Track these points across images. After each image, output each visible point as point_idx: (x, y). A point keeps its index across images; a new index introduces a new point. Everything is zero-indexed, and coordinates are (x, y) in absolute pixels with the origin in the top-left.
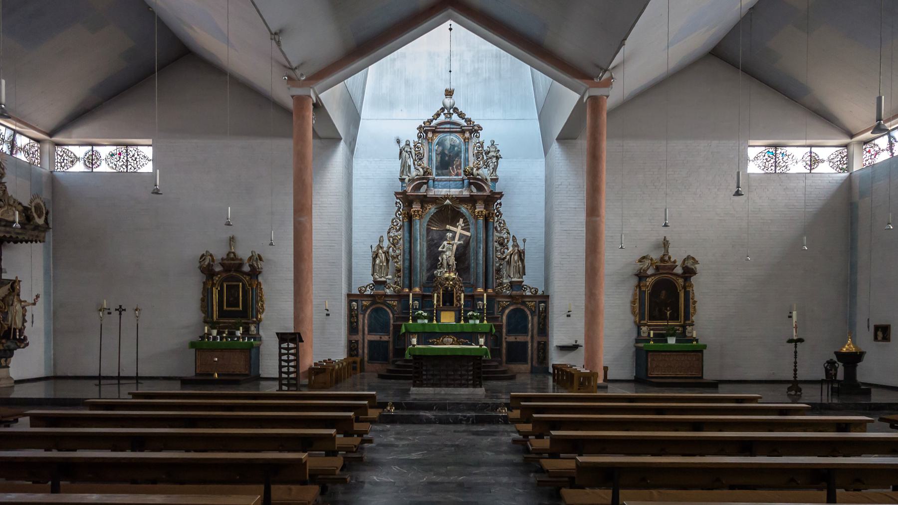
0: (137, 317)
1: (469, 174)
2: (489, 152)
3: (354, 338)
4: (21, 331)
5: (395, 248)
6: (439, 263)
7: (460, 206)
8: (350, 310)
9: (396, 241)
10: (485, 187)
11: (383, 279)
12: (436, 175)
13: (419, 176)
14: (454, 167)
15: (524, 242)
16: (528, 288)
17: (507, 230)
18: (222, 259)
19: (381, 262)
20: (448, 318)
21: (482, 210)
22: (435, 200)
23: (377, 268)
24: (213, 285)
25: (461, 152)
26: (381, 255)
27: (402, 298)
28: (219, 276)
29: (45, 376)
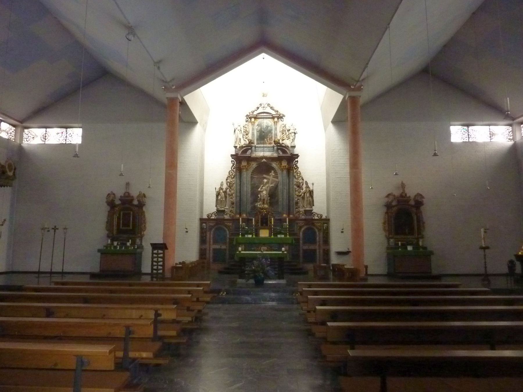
1: (277, 143)
2: (290, 130)
3: (204, 247)
6: (259, 199)
7: (272, 163)
9: (231, 185)
11: (223, 209)
12: (257, 144)
14: (268, 139)
15: (313, 185)
16: (316, 214)
17: (302, 177)
18: (121, 197)
19: (222, 198)
20: (264, 233)
22: (256, 159)
23: (219, 202)
25: (272, 130)
26: (222, 194)
27: (235, 221)
28: (118, 207)
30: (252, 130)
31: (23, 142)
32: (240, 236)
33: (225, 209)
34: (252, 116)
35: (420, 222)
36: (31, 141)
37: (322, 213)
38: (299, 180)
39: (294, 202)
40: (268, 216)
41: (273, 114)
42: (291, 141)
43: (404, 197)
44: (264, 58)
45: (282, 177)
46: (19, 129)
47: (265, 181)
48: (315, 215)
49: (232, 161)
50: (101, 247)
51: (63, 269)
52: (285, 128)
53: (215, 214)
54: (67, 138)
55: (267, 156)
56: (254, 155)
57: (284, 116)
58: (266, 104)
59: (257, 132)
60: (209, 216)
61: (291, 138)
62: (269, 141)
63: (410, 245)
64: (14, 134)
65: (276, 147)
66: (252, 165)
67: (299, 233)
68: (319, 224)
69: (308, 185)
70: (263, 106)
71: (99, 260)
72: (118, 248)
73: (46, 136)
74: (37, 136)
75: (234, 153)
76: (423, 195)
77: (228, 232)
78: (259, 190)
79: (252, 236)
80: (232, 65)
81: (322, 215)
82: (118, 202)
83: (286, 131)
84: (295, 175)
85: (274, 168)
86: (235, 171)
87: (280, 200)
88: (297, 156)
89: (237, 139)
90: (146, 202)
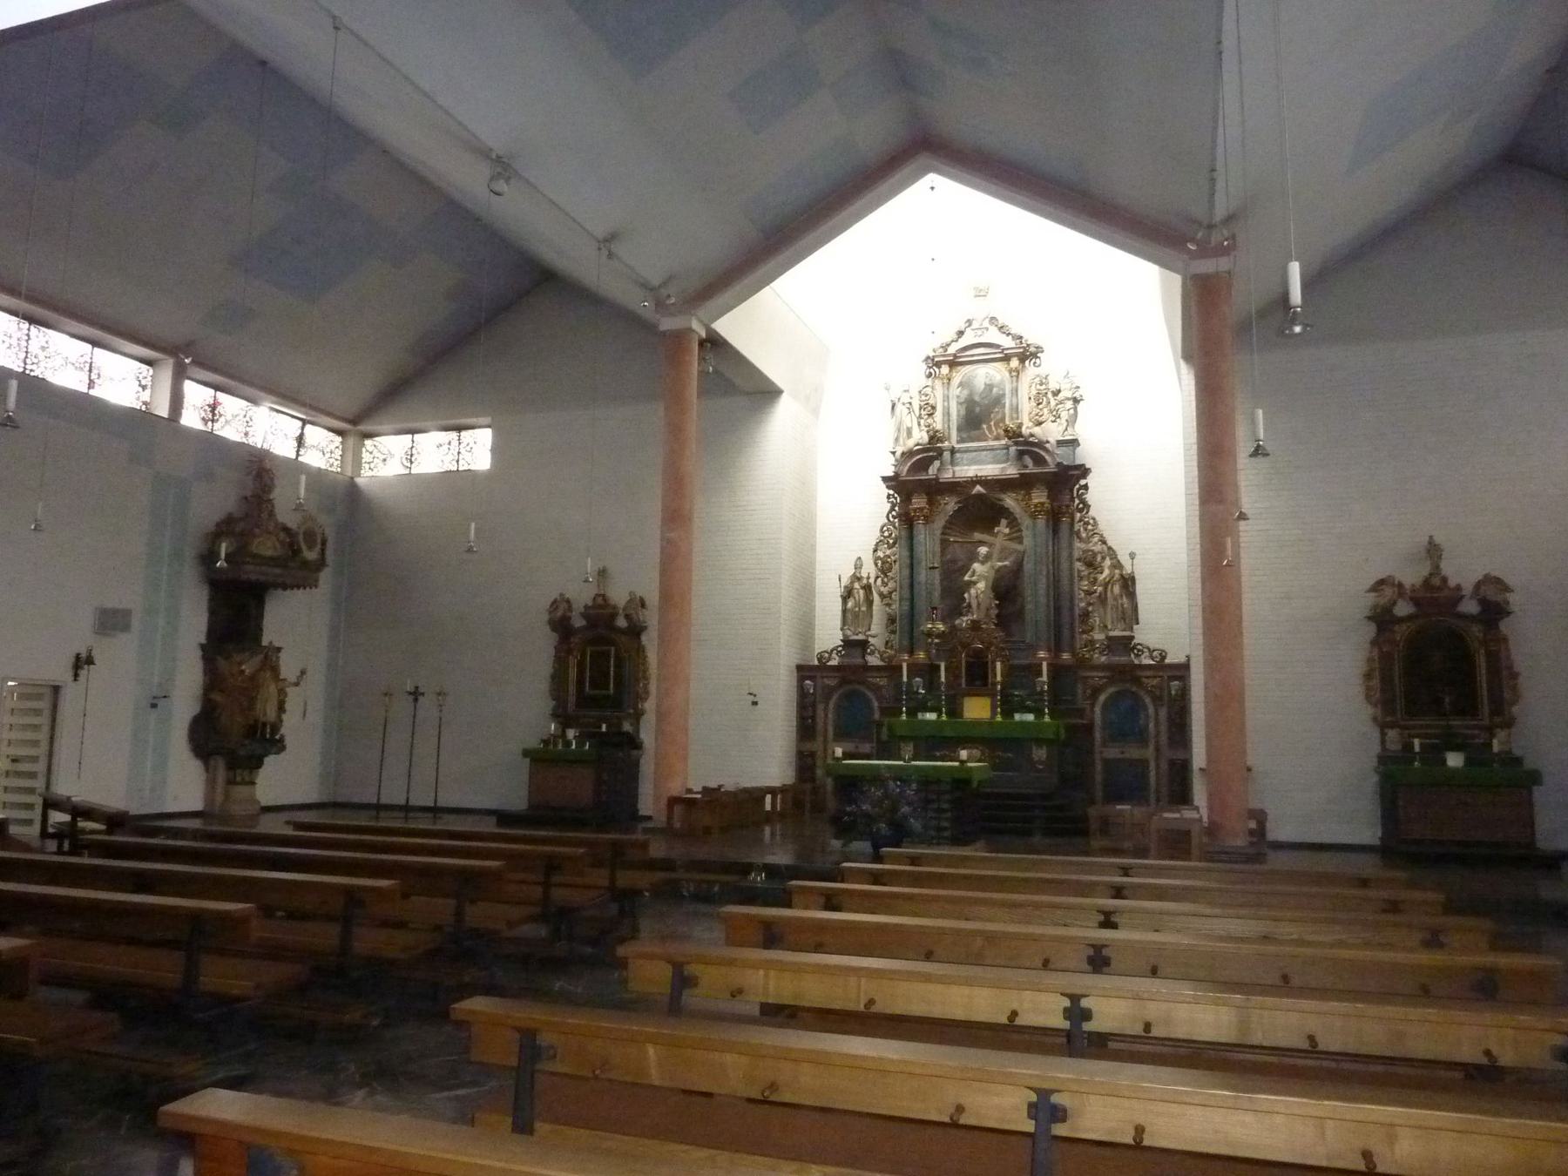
0: (386, 706)
1: (1014, 435)
2: (1059, 391)
3: (808, 746)
4: (276, 727)
5: (886, 580)
6: (965, 605)
7: (1003, 496)
8: (802, 693)
9: (887, 565)
10: (1047, 457)
11: (861, 637)
12: (958, 442)
13: (921, 445)
14: (992, 423)
15: (1133, 559)
16: (1145, 650)
17: (1102, 536)
18: (586, 607)
19: (857, 604)
20: (977, 709)
21: (1042, 500)
22: (955, 487)
23: (849, 616)
24: (569, 652)
25: (1004, 395)
26: (858, 593)
27: (892, 669)
29: (318, 801)
30: (944, 401)
31: (362, 472)
32: (904, 717)
33: (868, 636)
34: (942, 359)
35: (1503, 674)
36: (379, 468)
37: (1165, 647)
38: (1091, 544)
39: (1077, 612)
40: (987, 657)
41: (1007, 347)
42: (1065, 424)
43: (1439, 589)
44: (932, 188)
45: (1034, 534)
46: (351, 441)
47: (983, 550)
48: (1143, 652)
49: (889, 496)
50: (534, 743)
51: (408, 799)
52: (1044, 387)
53: (840, 652)
54: (461, 457)
55: (986, 476)
56: (947, 476)
57: (1039, 349)
58: (985, 319)
59: (959, 406)
60: (822, 657)
61: (1064, 415)
62: (994, 429)
63: (1457, 748)
64: (340, 453)
65: (1014, 448)
66: (945, 504)
67: (1092, 711)
68: (1155, 682)
69: (1116, 558)
70: (975, 325)
71: (525, 778)
72: (574, 747)
73: (412, 455)
74: (392, 456)
75: (890, 472)
76: (1510, 580)
77: (876, 704)
78: (966, 578)
79: (939, 716)
80: (844, 214)
81: (1166, 653)
82: (578, 622)
83: (1050, 395)
84: (1079, 530)
85: (1012, 510)
86: (897, 524)
87: (1029, 607)
88: (1084, 471)
89: (899, 430)
90: (645, 622)
